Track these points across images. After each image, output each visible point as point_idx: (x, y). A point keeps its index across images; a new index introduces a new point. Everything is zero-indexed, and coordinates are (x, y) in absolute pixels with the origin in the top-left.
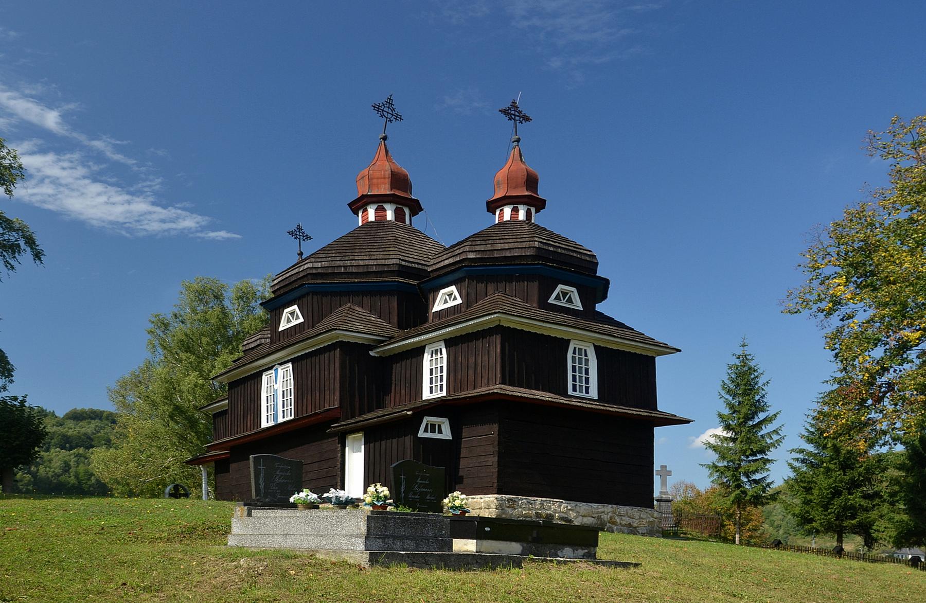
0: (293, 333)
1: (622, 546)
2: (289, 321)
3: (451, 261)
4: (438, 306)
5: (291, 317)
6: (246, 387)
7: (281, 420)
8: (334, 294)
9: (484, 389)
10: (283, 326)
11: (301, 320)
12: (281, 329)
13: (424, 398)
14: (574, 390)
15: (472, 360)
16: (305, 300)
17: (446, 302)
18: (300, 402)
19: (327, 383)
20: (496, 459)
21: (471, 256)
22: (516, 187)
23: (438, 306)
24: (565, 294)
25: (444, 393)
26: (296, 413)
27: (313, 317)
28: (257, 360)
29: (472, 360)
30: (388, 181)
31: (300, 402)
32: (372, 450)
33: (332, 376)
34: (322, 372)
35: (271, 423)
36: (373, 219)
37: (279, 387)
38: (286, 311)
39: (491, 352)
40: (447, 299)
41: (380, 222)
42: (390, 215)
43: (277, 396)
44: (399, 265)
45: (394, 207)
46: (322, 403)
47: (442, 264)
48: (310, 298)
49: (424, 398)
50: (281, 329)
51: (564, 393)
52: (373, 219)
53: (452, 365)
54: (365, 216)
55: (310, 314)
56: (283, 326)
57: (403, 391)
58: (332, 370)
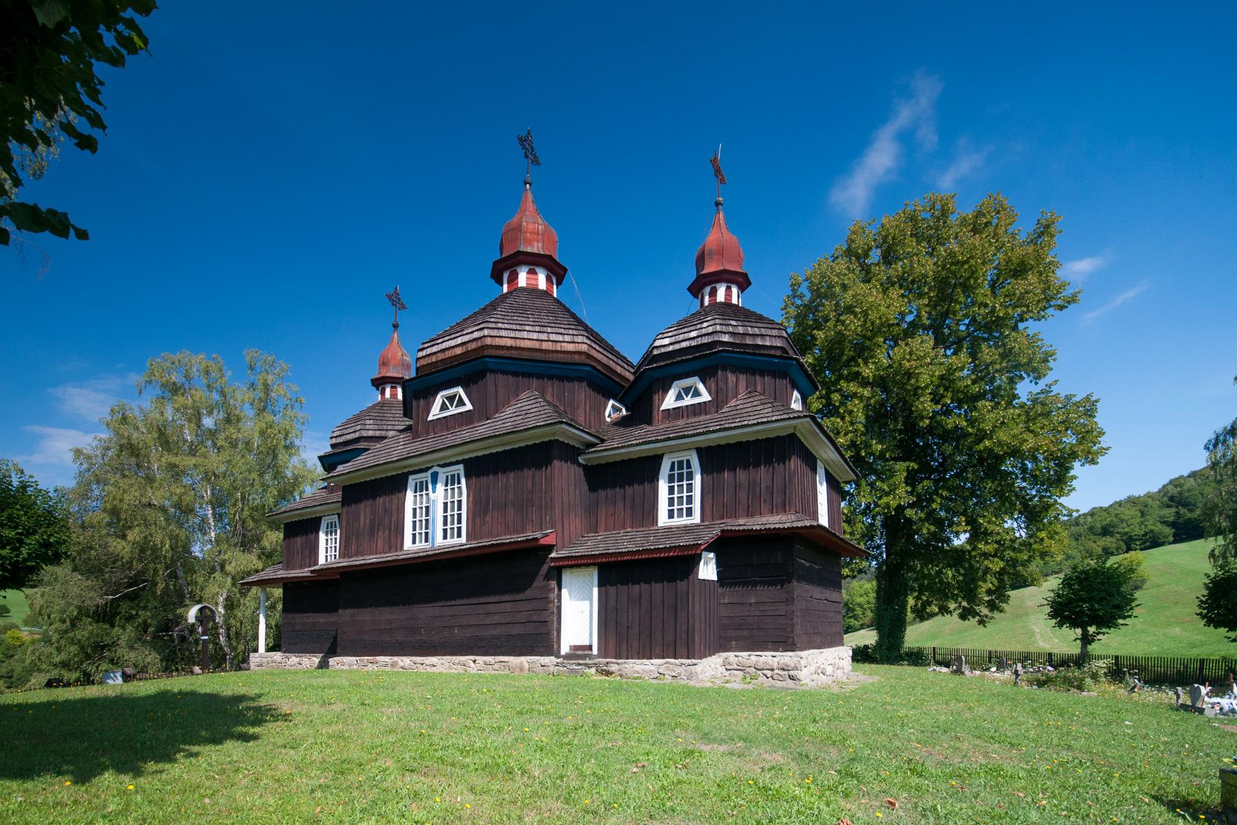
7: (439, 541)
13: (660, 524)
14: (671, 515)
21: (726, 338)
35: (421, 545)
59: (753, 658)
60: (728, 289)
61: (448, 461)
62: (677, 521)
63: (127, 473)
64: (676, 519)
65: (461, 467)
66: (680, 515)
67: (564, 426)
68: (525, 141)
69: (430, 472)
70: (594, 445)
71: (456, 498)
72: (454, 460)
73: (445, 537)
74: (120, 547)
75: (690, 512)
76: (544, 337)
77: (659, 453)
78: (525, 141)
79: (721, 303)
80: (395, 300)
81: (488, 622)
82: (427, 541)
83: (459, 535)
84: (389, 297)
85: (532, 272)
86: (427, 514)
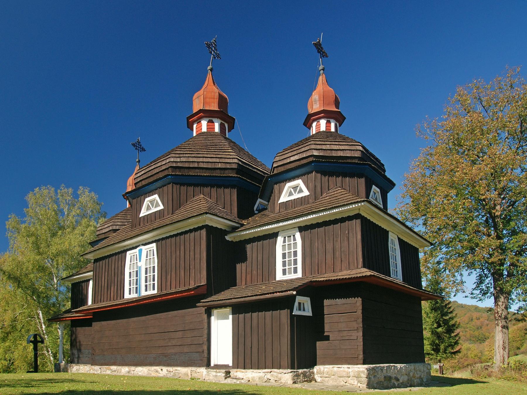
0: (153, 218)
1: (359, 385)
2: (148, 208)
3: (296, 157)
4: (284, 198)
5: (152, 204)
6: (110, 265)
7: (144, 293)
8: (196, 185)
9: (345, 272)
10: (143, 213)
11: (161, 207)
12: (141, 215)
13: (278, 279)
15: (329, 247)
16: (165, 188)
17: (291, 194)
18: (164, 278)
19: (192, 263)
20: (361, 334)
21: (316, 153)
22: (328, 104)
23: (284, 198)
24: (295, 188)
25: (299, 274)
26: (160, 288)
27: (174, 205)
28: (124, 241)
29: (329, 247)
30: (217, 101)
31: (164, 278)
32: (241, 324)
33: (197, 256)
34: (187, 253)
35: (134, 296)
36: (206, 131)
37: (142, 264)
38: (147, 199)
39: (351, 239)
40: (294, 190)
41: (210, 132)
42: (217, 129)
43: (141, 271)
44: (238, 163)
45: (220, 121)
46: (187, 280)
47: (288, 161)
48: (170, 185)
49: (278, 279)
50: (141, 215)
51: (390, 276)
52: (206, 131)
53: (308, 250)
54: (199, 128)
55: (170, 202)
56: (143, 213)
57: (255, 272)
58: (198, 251)
59: (335, 369)
60: (328, 122)
61: (147, 242)
62: (288, 277)
63: (518, 331)
64: (287, 275)
65: (154, 245)
66: (290, 273)
67: (208, 215)
68: (318, 47)
69: (138, 249)
70: (238, 228)
71: (152, 266)
72: (150, 241)
73: (146, 290)
74: (517, 385)
75: (295, 271)
76: (178, 160)
77: (276, 231)
78: (318, 47)
79: (323, 132)
80: (138, 147)
81: (170, 344)
82: (136, 293)
83: (154, 289)
84: (134, 145)
85: (211, 122)
86: (137, 276)
